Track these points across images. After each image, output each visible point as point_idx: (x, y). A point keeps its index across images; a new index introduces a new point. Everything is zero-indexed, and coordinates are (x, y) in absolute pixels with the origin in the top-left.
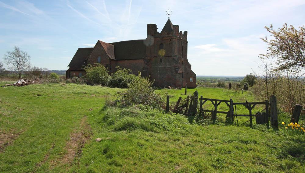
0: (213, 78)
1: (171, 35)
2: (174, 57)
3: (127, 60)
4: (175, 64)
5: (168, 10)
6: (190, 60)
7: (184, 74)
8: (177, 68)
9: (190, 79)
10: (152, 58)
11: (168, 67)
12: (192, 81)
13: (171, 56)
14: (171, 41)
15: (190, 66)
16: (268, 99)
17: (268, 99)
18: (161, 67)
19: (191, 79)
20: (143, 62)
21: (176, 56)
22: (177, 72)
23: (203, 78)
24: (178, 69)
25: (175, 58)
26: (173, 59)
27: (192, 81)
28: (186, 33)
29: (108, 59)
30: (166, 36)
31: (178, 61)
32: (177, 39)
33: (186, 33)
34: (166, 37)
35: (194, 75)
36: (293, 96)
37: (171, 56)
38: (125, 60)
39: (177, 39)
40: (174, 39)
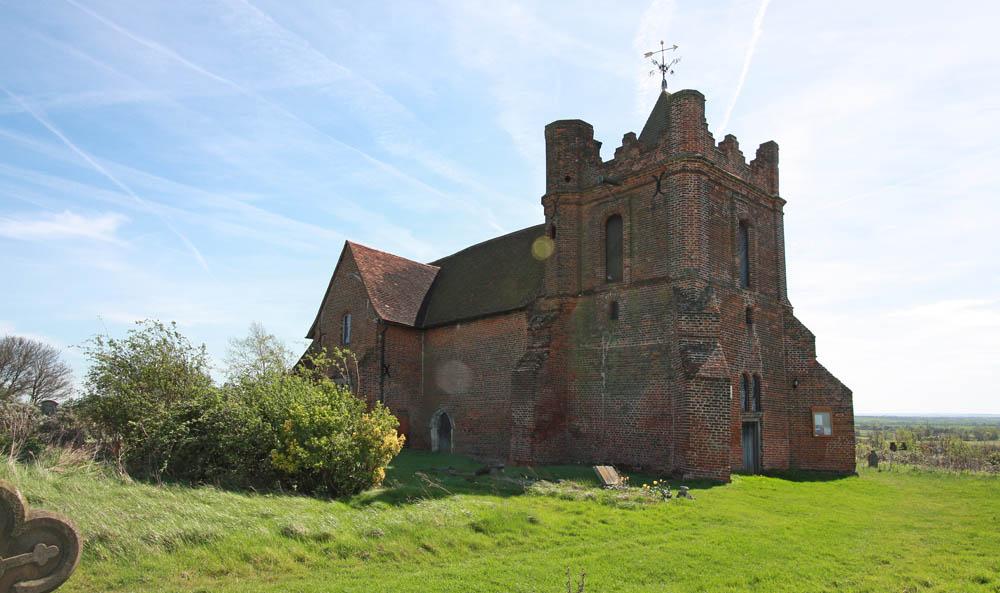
0: (984, 424)
1: (661, 157)
2: (682, 278)
3: (462, 321)
4: (685, 325)
5: (655, 47)
6: (801, 314)
7: (765, 385)
8: (695, 349)
9: (811, 420)
10: (571, 300)
11: (651, 343)
12: (828, 431)
13: (666, 279)
14: (658, 190)
15: (805, 340)
16: (67, 466)
17: (67, 466)
18: (614, 345)
19: (819, 419)
20: (525, 325)
21: (690, 275)
22: (690, 371)
23: (942, 421)
24: (706, 349)
25: (684, 285)
26: (676, 290)
27: (828, 431)
28: (769, 153)
29: (375, 321)
30: (636, 168)
31: (709, 299)
32: (692, 171)
33: (769, 153)
34: (635, 174)
35: (839, 397)
36: (360, 535)
37: (666, 279)
38: (453, 324)
39: (692, 171)
40: (674, 173)
